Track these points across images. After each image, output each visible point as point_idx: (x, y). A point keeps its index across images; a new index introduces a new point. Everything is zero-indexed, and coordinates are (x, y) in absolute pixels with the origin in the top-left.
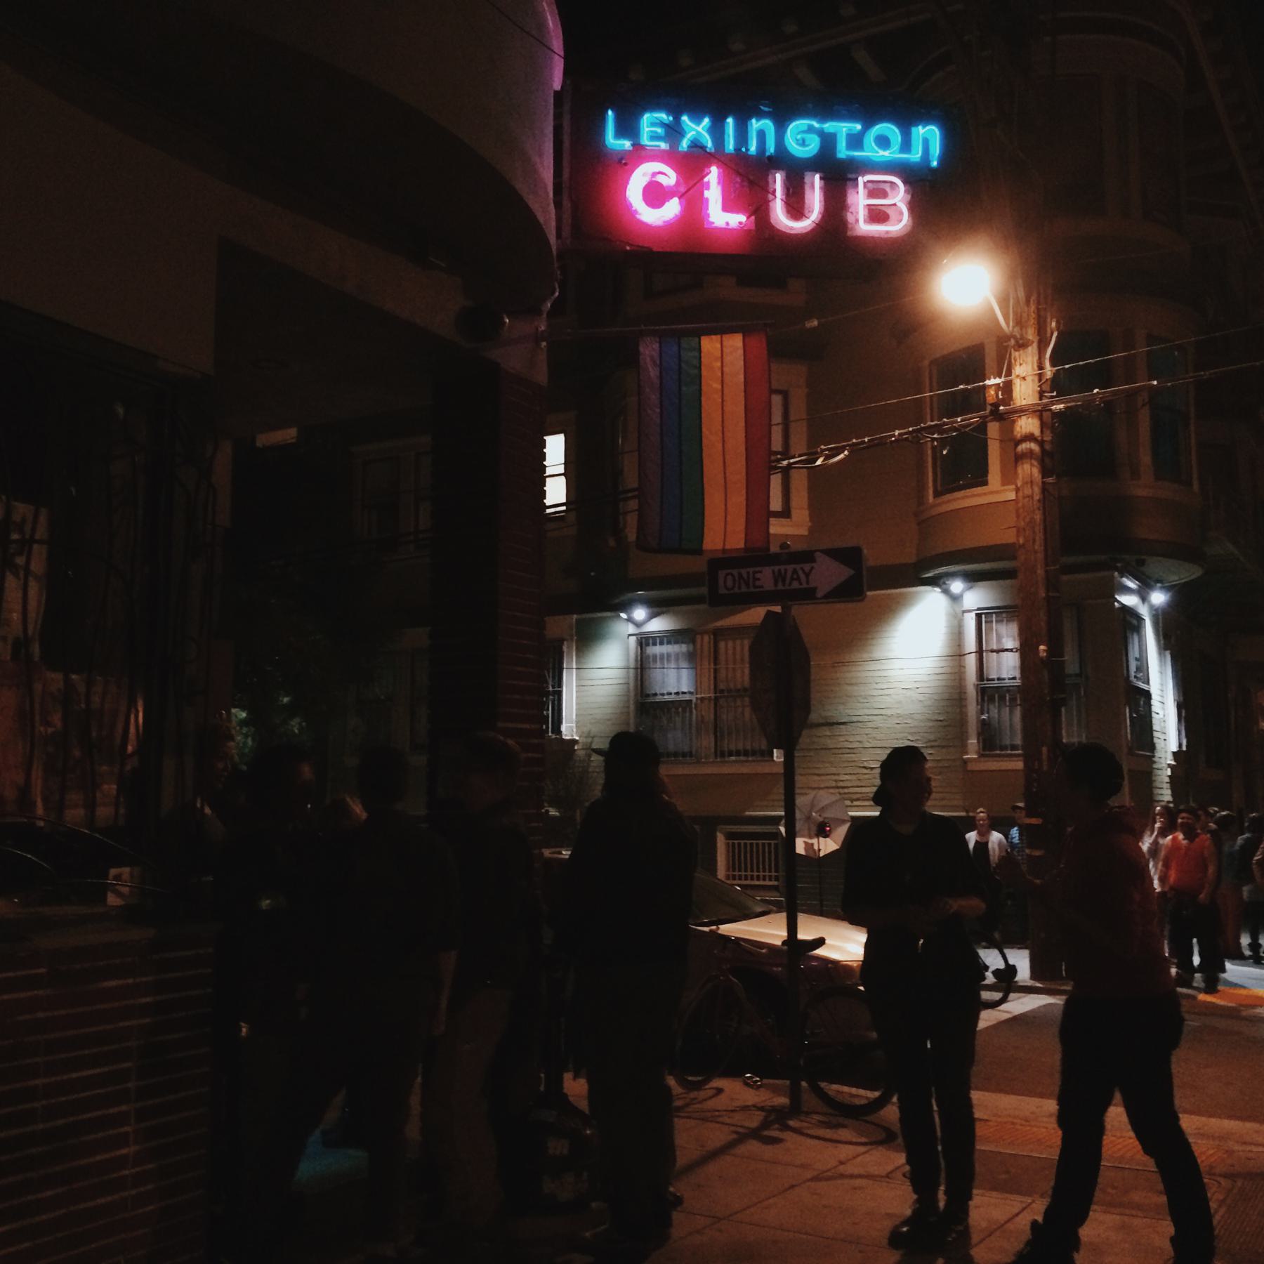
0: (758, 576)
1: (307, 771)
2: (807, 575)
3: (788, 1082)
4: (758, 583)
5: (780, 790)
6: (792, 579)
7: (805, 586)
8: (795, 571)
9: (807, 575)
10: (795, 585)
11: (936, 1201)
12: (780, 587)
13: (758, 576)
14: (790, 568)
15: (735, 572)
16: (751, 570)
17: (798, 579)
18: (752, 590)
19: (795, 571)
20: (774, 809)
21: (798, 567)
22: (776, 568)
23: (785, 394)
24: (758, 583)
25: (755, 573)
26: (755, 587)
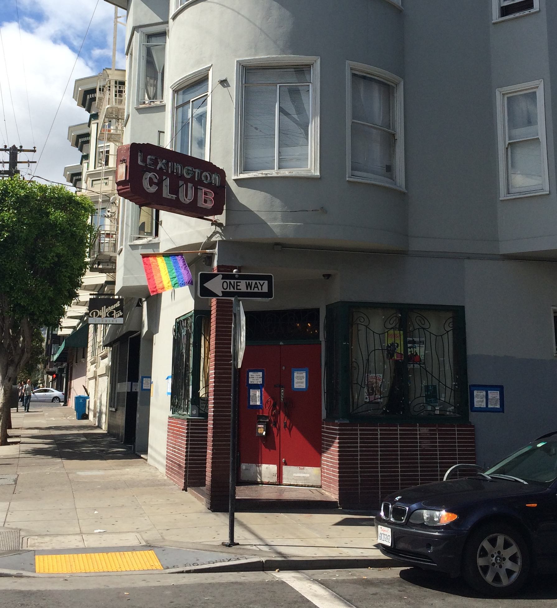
0: (238, 284)
1: (261, 430)
2: (262, 286)
3: (236, 498)
4: (238, 288)
5: (151, 259)
6: (255, 287)
7: (260, 291)
8: (256, 283)
9: (262, 286)
10: (256, 290)
11: (285, 392)
12: (249, 290)
13: (238, 284)
14: (254, 282)
15: (228, 281)
16: (236, 281)
17: (257, 287)
18: (236, 290)
19: (256, 283)
20: (127, 270)
21: (257, 281)
22: (248, 281)
23: (268, 295)
24: (238, 288)
25: (237, 282)
26: (237, 289)
